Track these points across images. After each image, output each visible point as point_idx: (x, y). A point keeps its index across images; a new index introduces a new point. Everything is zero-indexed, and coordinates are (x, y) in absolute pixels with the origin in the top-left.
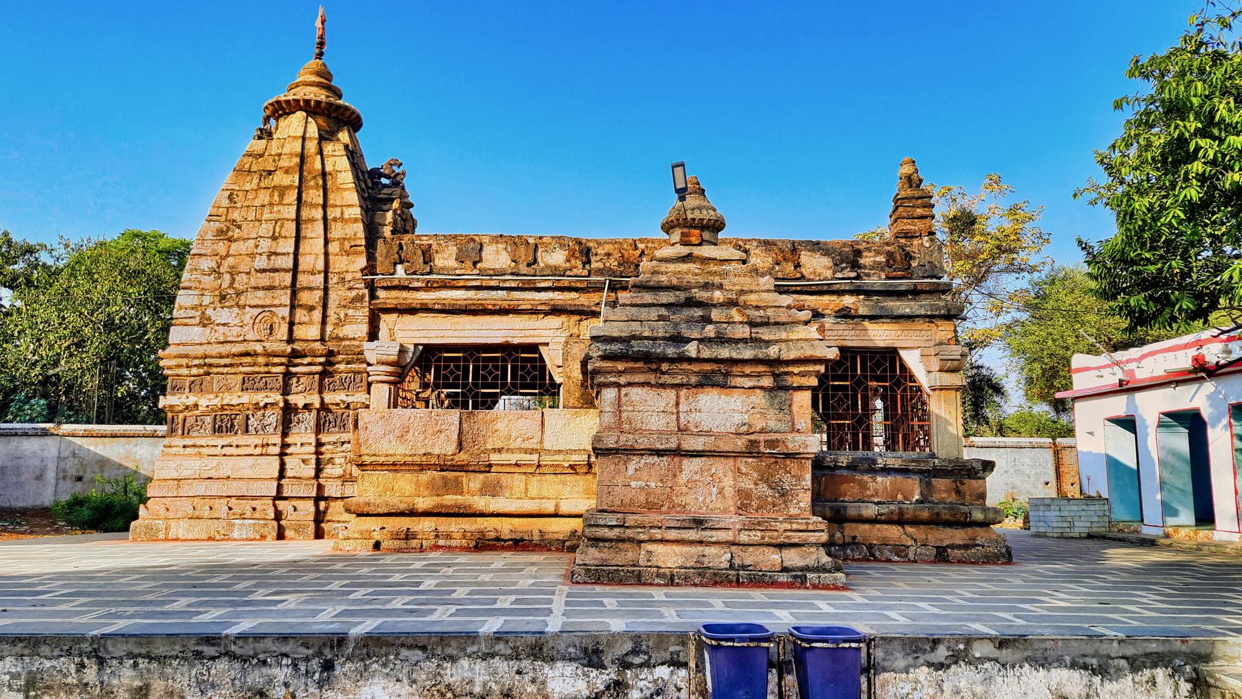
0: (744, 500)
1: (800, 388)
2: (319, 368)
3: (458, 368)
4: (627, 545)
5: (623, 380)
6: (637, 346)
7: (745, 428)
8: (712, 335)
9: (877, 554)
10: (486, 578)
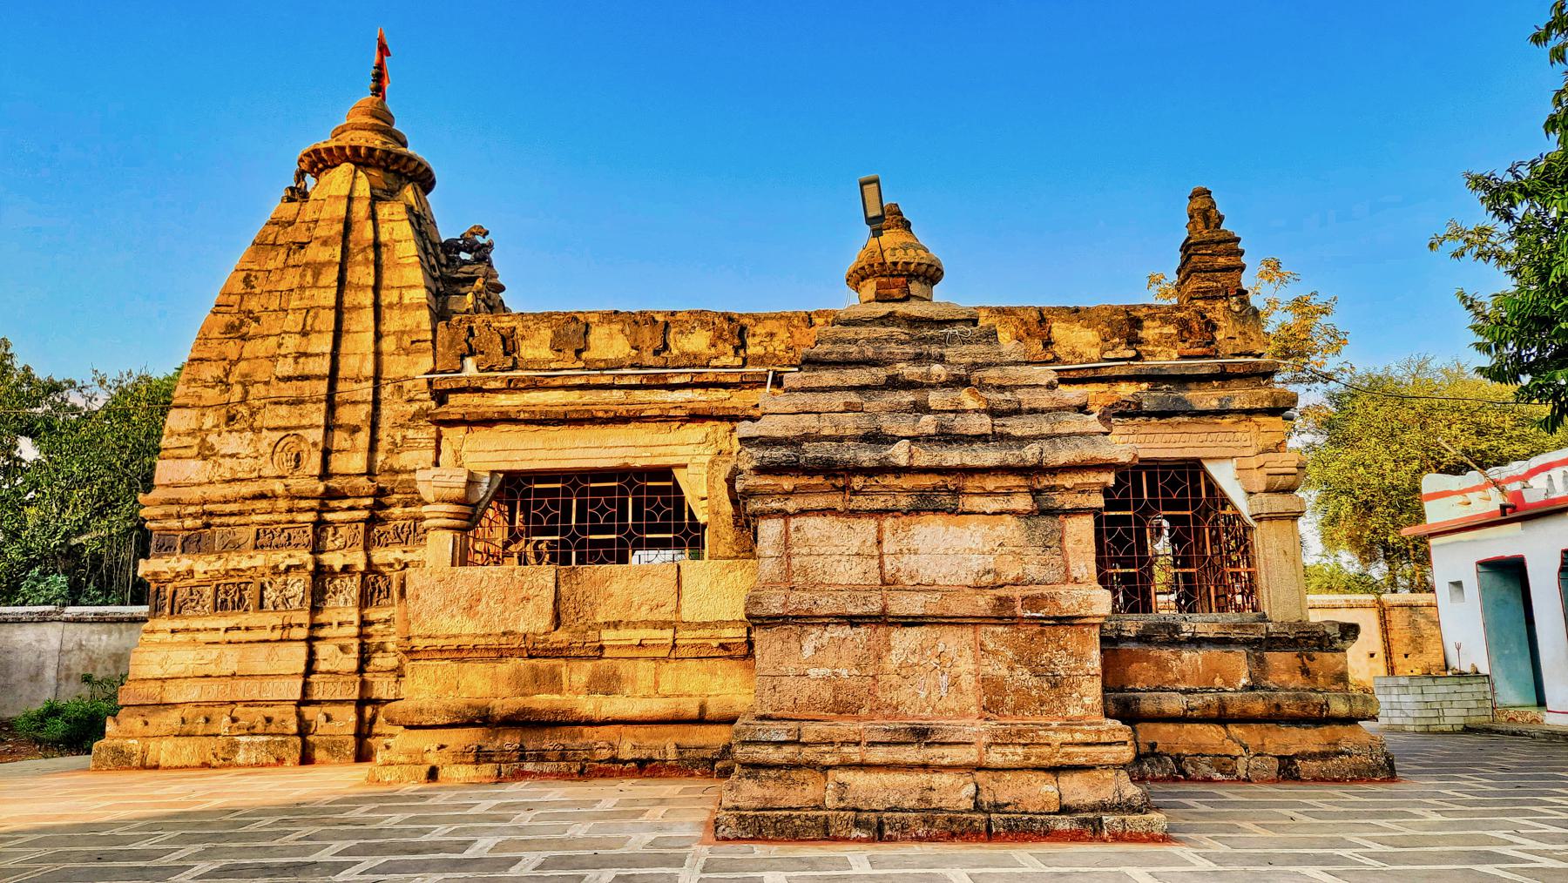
0: (993, 699)
1: (1076, 511)
2: (365, 514)
3: (554, 505)
4: (804, 774)
5: (791, 506)
6: (812, 451)
7: (989, 578)
8: (931, 430)
9: (1190, 769)
10: (579, 830)
